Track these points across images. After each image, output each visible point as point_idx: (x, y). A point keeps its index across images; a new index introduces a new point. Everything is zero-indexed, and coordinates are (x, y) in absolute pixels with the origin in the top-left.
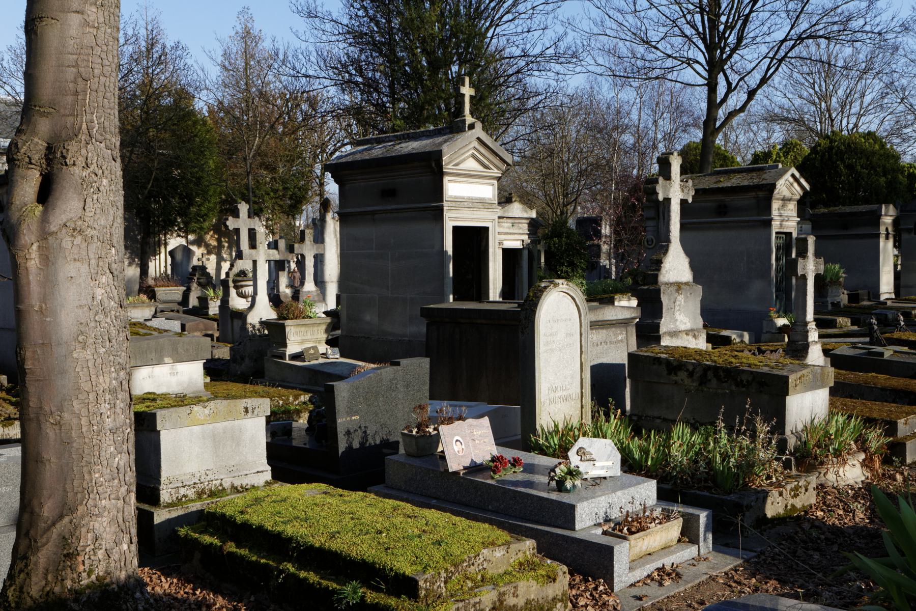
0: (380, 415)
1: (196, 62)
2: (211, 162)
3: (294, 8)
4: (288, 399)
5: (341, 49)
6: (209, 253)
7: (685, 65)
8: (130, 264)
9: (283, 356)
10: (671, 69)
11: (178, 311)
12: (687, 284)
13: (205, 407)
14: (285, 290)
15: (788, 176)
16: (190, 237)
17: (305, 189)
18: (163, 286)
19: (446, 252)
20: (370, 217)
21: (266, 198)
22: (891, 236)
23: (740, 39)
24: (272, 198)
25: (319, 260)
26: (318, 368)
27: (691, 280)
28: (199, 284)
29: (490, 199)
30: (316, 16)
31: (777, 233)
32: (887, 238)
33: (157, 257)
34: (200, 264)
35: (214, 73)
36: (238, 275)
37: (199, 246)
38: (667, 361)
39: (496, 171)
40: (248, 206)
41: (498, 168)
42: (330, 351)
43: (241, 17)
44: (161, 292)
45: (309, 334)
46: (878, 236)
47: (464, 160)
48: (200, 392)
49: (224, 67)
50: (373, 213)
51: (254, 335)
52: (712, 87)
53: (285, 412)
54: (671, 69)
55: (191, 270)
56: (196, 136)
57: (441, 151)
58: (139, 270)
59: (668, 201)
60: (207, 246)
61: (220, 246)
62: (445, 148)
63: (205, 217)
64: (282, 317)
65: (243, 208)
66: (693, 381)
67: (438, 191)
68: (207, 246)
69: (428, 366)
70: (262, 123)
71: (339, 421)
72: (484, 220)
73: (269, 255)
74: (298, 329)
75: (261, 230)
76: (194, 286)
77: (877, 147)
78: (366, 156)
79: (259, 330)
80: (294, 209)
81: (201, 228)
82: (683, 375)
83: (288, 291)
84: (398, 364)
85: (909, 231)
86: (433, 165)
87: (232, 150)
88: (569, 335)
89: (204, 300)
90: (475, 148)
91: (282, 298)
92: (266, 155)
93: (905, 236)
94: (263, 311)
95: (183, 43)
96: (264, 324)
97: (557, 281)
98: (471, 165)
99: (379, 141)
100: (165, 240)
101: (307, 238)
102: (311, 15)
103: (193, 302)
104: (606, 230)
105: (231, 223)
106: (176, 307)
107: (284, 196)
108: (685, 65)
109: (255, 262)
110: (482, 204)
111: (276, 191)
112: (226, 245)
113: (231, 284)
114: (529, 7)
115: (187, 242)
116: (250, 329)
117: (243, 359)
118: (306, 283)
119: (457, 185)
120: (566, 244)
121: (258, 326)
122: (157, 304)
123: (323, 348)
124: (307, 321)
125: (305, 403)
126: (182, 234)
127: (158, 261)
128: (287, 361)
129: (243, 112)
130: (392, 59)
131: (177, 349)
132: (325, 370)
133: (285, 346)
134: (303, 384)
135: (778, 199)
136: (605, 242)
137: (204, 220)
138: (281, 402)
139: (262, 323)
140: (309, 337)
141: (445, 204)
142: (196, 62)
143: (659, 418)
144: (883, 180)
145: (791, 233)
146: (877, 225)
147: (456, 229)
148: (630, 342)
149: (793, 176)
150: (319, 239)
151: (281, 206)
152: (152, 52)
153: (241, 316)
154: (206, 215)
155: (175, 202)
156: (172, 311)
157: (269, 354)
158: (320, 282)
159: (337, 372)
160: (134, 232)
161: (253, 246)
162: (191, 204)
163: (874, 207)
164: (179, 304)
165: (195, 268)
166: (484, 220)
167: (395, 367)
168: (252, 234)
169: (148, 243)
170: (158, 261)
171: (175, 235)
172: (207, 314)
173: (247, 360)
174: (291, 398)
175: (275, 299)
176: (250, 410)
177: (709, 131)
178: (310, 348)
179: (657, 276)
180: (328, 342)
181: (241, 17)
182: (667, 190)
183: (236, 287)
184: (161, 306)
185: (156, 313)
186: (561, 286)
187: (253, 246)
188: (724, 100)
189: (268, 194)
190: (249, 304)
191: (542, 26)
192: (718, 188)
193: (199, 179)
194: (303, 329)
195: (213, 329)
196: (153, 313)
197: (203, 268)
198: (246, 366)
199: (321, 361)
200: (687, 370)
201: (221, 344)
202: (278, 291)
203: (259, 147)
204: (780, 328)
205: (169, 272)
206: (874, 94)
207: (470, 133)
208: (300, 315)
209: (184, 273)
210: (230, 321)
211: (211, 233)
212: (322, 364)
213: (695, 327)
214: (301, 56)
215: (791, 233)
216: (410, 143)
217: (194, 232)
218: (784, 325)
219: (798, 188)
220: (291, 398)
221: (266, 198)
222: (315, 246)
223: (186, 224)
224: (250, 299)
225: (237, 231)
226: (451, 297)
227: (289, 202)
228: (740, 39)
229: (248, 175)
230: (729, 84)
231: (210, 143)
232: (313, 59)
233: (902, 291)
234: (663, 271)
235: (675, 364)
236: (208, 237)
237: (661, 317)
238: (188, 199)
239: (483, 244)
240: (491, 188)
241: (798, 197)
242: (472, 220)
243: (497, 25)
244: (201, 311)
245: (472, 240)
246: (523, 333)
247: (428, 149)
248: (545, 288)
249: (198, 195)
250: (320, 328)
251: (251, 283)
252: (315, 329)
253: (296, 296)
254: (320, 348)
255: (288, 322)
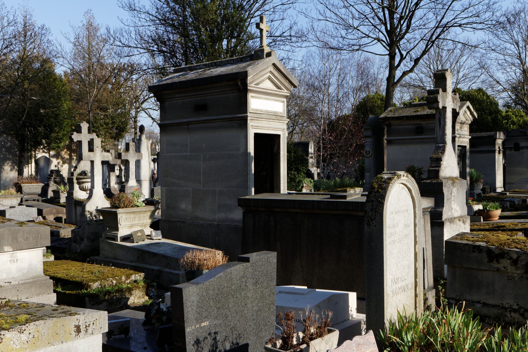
0: (230, 318)
1: (56, 40)
2: (65, 105)
3: (120, 5)
4: (121, 279)
5: (150, 30)
6: (64, 163)
7: (376, 41)
8: (11, 170)
9: (115, 238)
10: (366, 45)
11: (38, 201)
12: (456, 178)
13: (21, 332)
14: (114, 185)
15: (465, 108)
16: (51, 152)
17: (126, 123)
18: (27, 183)
19: (250, 153)
20: (186, 127)
21: (101, 128)
22: (501, 152)
23: (408, 26)
24: (105, 128)
25: (138, 163)
26: (145, 249)
27: (459, 176)
28: (55, 182)
29: (281, 113)
30: (135, 10)
31: (459, 146)
32: (499, 153)
33: (30, 165)
34: (57, 168)
35: (68, 48)
36: (80, 174)
37: (57, 158)
38: (489, 251)
39: (286, 91)
40: (88, 125)
41: (287, 89)
42: (154, 234)
43: (86, 15)
44: (26, 187)
45: (136, 219)
46: (494, 151)
47: (263, 81)
48: (39, 277)
49: (75, 45)
50: (188, 123)
51: (91, 220)
52: (392, 57)
53: (118, 291)
54: (366, 45)
55: (50, 173)
56: (55, 88)
57: (247, 72)
58: (17, 173)
59: (444, 108)
60: (63, 158)
61: (71, 158)
62: (250, 70)
63: (61, 140)
64: (114, 206)
65: (85, 126)
66: (517, 269)
67: (242, 105)
68: (63, 158)
69: (275, 261)
70: (98, 81)
71: (188, 330)
72: (277, 129)
73: (104, 157)
74: (128, 216)
75: (98, 142)
76: (52, 183)
77: (485, 97)
78: (182, 79)
79: (95, 216)
80: (118, 135)
81: (59, 147)
82: (505, 263)
83: (116, 186)
84: (247, 260)
85: (510, 149)
86: (239, 84)
87: (79, 98)
88: (406, 226)
89: (57, 193)
90: (271, 72)
91: (113, 191)
92: (101, 101)
93: (508, 152)
94: (98, 202)
95: (47, 26)
96: (100, 211)
97: (399, 173)
98: (268, 85)
99: (191, 69)
100: (35, 155)
101: (131, 149)
102: (132, 8)
103: (50, 194)
104: (311, 150)
105: (76, 137)
106: (37, 197)
107: (112, 127)
108: (376, 41)
109: (92, 162)
110: (275, 116)
111: (107, 124)
112: (75, 158)
113: (75, 181)
114: (272, 7)
115: (50, 156)
116: (88, 216)
117: (82, 239)
118: (130, 181)
119: (257, 100)
120: (294, 157)
121: (94, 213)
122: (22, 195)
123: (148, 231)
124: (135, 209)
125: (135, 281)
126: (46, 151)
127: (30, 168)
128: (119, 242)
129: (88, 76)
130: (185, 35)
131: (16, 238)
132: (151, 250)
133: (117, 229)
134: (132, 262)
135: (458, 123)
136: (312, 157)
137: (61, 142)
138: (114, 282)
139: (98, 211)
140: (137, 222)
141: (249, 114)
142: (56, 40)
143: (479, 302)
144: (489, 118)
145: (466, 147)
146: (494, 144)
147: (257, 135)
148: (426, 229)
149: (468, 108)
150: (138, 149)
151: (110, 133)
152: (27, 32)
153: (81, 204)
154: (61, 138)
155: (41, 129)
156: (34, 200)
157: (103, 236)
158: (139, 181)
159: (161, 252)
160: (14, 150)
161: (91, 149)
162: (52, 131)
163: (492, 133)
164: (39, 195)
165: (52, 171)
166: (277, 129)
167: (245, 264)
168: (91, 143)
169: (23, 156)
170: (30, 168)
171: (41, 151)
172: (59, 202)
173: (85, 241)
174: (123, 278)
175: (108, 193)
176: (82, 328)
177: (391, 84)
178: (137, 231)
179: (438, 172)
180: (151, 227)
181: (86, 15)
182: (444, 101)
183: (79, 183)
184: (26, 197)
185: (21, 201)
186: (402, 177)
187: (91, 149)
188: (399, 65)
189: (102, 126)
190: (87, 196)
191: (281, 17)
192: (418, 115)
193: (57, 115)
194: (132, 216)
195: (63, 213)
196: (19, 201)
197: (58, 172)
198: (85, 244)
199: (147, 242)
200: (511, 258)
201: (67, 225)
202: (109, 186)
203: (96, 96)
204: (476, 212)
205: (34, 173)
206: (465, 71)
207: (268, 59)
208: (130, 204)
209: (45, 175)
210: (74, 208)
211: (65, 150)
212: (148, 245)
213: (463, 214)
214: (125, 34)
215: (466, 147)
216: (218, 69)
217: (53, 149)
218: (479, 210)
219: (470, 116)
220: (123, 278)
221: (101, 128)
222: (137, 154)
223: (49, 144)
224: (88, 192)
225: (80, 142)
226: (253, 189)
227: (115, 131)
228: (408, 26)
229: (89, 113)
230: (401, 55)
231: (64, 92)
232: (134, 37)
233: (507, 186)
234: (443, 167)
235: (497, 252)
236: (63, 153)
237: (443, 206)
238: (50, 129)
239: (276, 148)
240: (282, 104)
241: (470, 122)
242: (268, 128)
243: (252, 17)
244: (55, 200)
245: (267, 143)
246: (369, 225)
247: (235, 71)
248: (390, 179)
249: (56, 126)
250: (145, 215)
251: (89, 180)
252: (142, 215)
253: (122, 189)
254: (145, 231)
255: (119, 211)
